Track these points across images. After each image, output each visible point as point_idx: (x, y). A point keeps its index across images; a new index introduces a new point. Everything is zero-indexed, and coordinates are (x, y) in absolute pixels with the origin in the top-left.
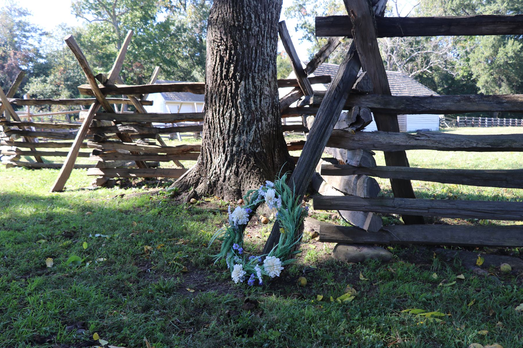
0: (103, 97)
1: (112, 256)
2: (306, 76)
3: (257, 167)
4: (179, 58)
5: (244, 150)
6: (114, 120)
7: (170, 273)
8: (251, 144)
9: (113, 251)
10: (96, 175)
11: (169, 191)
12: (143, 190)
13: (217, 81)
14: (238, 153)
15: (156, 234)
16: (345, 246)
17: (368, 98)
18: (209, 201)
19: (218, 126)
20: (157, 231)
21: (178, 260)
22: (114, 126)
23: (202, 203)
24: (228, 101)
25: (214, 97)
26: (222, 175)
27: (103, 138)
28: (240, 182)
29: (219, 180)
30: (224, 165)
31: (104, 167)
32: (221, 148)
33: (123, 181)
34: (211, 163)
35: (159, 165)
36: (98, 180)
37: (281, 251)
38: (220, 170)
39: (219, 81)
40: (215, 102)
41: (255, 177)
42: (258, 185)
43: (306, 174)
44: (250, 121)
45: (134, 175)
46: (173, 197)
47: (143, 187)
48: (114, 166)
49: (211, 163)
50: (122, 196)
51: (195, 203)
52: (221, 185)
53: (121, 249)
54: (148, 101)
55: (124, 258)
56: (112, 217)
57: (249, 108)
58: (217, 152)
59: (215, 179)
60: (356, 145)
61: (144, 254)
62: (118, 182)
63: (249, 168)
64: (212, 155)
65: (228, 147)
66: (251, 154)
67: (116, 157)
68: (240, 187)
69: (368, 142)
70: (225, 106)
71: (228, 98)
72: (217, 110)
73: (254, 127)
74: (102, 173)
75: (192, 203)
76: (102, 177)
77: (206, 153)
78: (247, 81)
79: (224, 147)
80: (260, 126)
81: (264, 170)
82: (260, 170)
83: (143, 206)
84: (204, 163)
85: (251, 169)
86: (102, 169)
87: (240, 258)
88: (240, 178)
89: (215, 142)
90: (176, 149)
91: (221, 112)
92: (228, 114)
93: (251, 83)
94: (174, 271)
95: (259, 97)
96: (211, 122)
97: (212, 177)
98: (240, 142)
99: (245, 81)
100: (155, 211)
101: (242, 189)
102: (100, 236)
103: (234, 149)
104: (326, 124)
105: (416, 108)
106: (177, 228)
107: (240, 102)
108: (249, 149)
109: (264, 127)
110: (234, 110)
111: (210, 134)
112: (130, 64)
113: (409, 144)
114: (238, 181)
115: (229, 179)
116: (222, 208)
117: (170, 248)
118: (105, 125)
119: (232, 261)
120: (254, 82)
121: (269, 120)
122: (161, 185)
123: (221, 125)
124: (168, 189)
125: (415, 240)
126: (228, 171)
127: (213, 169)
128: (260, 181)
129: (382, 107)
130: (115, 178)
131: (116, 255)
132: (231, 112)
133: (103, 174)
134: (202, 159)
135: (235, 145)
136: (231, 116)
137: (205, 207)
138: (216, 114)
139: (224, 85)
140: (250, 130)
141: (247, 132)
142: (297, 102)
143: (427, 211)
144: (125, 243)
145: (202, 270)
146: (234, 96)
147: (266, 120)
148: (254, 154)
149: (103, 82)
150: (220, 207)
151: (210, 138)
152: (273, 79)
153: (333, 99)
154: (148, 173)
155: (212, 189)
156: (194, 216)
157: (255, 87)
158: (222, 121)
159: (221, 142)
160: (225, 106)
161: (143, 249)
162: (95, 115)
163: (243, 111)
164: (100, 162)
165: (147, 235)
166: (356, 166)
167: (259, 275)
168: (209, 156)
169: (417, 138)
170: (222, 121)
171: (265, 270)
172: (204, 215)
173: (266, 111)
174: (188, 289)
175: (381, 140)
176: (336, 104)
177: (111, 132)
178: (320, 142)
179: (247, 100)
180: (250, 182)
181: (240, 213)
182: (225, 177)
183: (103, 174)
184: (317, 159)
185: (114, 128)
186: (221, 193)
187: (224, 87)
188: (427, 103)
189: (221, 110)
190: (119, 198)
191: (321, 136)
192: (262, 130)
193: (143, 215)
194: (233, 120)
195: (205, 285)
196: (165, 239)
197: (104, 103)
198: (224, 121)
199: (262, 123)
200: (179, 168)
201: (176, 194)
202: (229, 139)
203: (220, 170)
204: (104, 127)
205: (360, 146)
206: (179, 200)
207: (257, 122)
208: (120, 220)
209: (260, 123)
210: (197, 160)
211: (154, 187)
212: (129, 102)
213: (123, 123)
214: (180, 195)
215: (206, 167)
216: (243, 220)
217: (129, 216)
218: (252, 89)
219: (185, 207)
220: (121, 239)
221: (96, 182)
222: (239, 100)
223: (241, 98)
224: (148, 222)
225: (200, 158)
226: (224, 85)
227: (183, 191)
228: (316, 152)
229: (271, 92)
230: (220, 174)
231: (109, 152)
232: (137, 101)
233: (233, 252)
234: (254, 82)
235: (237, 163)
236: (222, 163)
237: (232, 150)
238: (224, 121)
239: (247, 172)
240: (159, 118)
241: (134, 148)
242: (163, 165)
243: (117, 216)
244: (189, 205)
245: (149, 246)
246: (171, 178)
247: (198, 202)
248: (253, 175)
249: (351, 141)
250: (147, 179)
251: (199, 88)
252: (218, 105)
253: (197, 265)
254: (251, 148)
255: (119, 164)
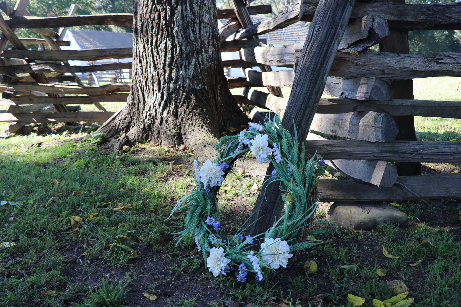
0: (11, 30)
1: (23, 238)
2: (245, 4)
3: (199, 107)
4: (93, 8)
5: (183, 87)
6: (26, 58)
7: (113, 263)
8: (190, 79)
9: (25, 228)
10: (8, 121)
11: (96, 138)
12: (64, 136)
13: (148, 6)
14: (177, 91)
15: (86, 195)
16: (346, 207)
17: (375, 7)
18: (145, 148)
19: (152, 60)
20: (86, 192)
21: (122, 240)
22: (26, 65)
23: (137, 150)
24: (162, 30)
25: (145, 25)
26: (158, 117)
27: (14, 78)
28: (180, 124)
29: (154, 123)
30: (160, 105)
31: (17, 112)
32: (155, 85)
33: (41, 127)
34: (144, 103)
35: (80, 109)
36: (11, 126)
37: (288, 228)
38: (156, 111)
39: (150, 6)
40: (147, 31)
41: (198, 119)
42: (202, 127)
43: (304, 112)
44: (189, 53)
45: (53, 120)
46: (100, 144)
47: (65, 133)
48: (30, 111)
49: (144, 103)
50: (40, 144)
51: (129, 151)
52: (158, 129)
53: (37, 225)
54: (65, 42)
55: (42, 240)
56: (25, 173)
57: (186, 37)
58: (151, 90)
59: (149, 122)
60: (359, 71)
61: (70, 228)
62: (36, 128)
63: (190, 108)
64: (145, 94)
65: (164, 84)
66: (192, 91)
67: (31, 100)
68: (180, 131)
69: (376, 68)
70: (159, 36)
71: (162, 26)
72: (150, 40)
73: (194, 60)
74: (16, 119)
75: (125, 152)
76: (15, 123)
77: (138, 91)
78: (184, 6)
79: (159, 84)
80: (200, 59)
81: (207, 110)
82: (202, 110)
83: (65, 157)
84: (135, 104)
85: (193, 109)
86: (15, 115)
87: (218, 238)
88: (180, 120)
89: (147, 79)
90: (101, 90)
91: (154, 43)
92: (162, 46)
93: (188, 8)
94: (119, 260)
95: (198, 25)
96: (143, 56)
97: (147, 119)
98: (177, 78)
99: (182, 6)
100: (82, 162)
101: (182, 133)
102: (8, 204)
103: (172, 86)
104: (329, 41)
105: (441, 20)
106: (112, 187)
107: (176, 31)
108: (189, 85)
109: (205, 60)
110: (169, 40)
111: (142, 70)
112: (45, 14)
113: (430, 69)
114: (178, 124)
115: (167, 121)
116: (162, 157)
117: (106, 219)
118: (16, 64)
119: (206, 242)
120: (192, 8)
121: (210, 53)
122: (84, 130)
123: (155, 58)
124: (94, 134)
125: (435, 195)
126: (165, 113)
127: (146, 110)
128: (204, 122)
129: (396, 19)
130: (32, 124)
131: (30, 235)
132: (166, 42)
133: (17, 120)
134: (133, 99)
135: (172, 82)
136: (166, 48)
137: (141, 156)
138: (148, 45)
139: (157, 11)
140: (189, 63)
141: (185, 66)
142: (233, 35)
143: (452, 158)
144: (43, 213)
145: (159, 252)
146: (169, 24)
147: (206, 52)
148: (195, 92)
149: (9, 13)
150: (160, 155)
151: (142, 74)
152: (213, 6)
153: (335, 5)
154: (68, 117)
155: (147, 133)
156: (130, 168)
157: (194, 13)
158: (155, 54)
159: (156, 78)
160: (159, 36)
161: (69, 221)
162: (3, 52)
163: (180, 41)
164: (12, 106)
165: (72, 198)
166: (363, 99)
167: (257, 268)
168: (141, 95)
169: (440, 61)
170: (155, 54)
171: (264, 258)
172: (143, 166)
173: (206, 42)
174: (146, 295)
175: (393, 64)
176: (339, 13)
177: (24, 72)
178: (322, 65)
179: (185, 28)
180: (192, 124)
181: (211, 170)
182: (162, 119)
183: (17, 120)
184: (319, 90)
185: (27, 67)
186: (158, 137)
187: (157, 13)
188: (455, 13)
189: (154, 41)
190: (35, 148)
191: (322, 56)
192: (203, 63)
193: (66, 169)
194: (169, 53)
195: (168, 283)
196: (98, 204)
197: (12, 38)
198: (158, 54)
199: (202, 55)
200: (101, 111)
201: (104, 140)
202: (165, 74)
203: (156, 111)
204: (14, 66)
205: (365, 72)
206: (109, 148)
207: (197, 54)
208: (36, 178)
209: (200, 56)
210: (126, 101)
211: (77, 133)
212: (44, 43)
213: (36, 61)
214: (110, 141)
215: (138, 108)
216: (217, 180)
217: (48, 171)
218: (190, 15)
219: (117, 157)
220: (38, 208)
221: (8, 128)
222: (176, 29)
223: (177, 26)
224: (73, 178)
225: (130, 98)
226: (157, 11)
227: (112, 136)
228: (316, 80)
229: (211, 20)
230: (156, 115)
231: (23, 95)
232: (53, 41)
233: (205, 227)
234: (192, 8)
235: (176, 102)
236: (157, 103)
237: (169, 88)
238: (158, 54)
239: (187, 113)
240: (78, 55)
241: (51, 89)
242: (85, 108)
243: (33, 172)
244: (122, 154)
245: (77, 214)
246: (95, 122)
247: (132, 149)
248: (195, 115)
249: (353, 66)
250: (68, 124)
251: (124, 20)
252: (150, 35)
253: (150, 245)
254: (191, 84)
255: (36, 109)
